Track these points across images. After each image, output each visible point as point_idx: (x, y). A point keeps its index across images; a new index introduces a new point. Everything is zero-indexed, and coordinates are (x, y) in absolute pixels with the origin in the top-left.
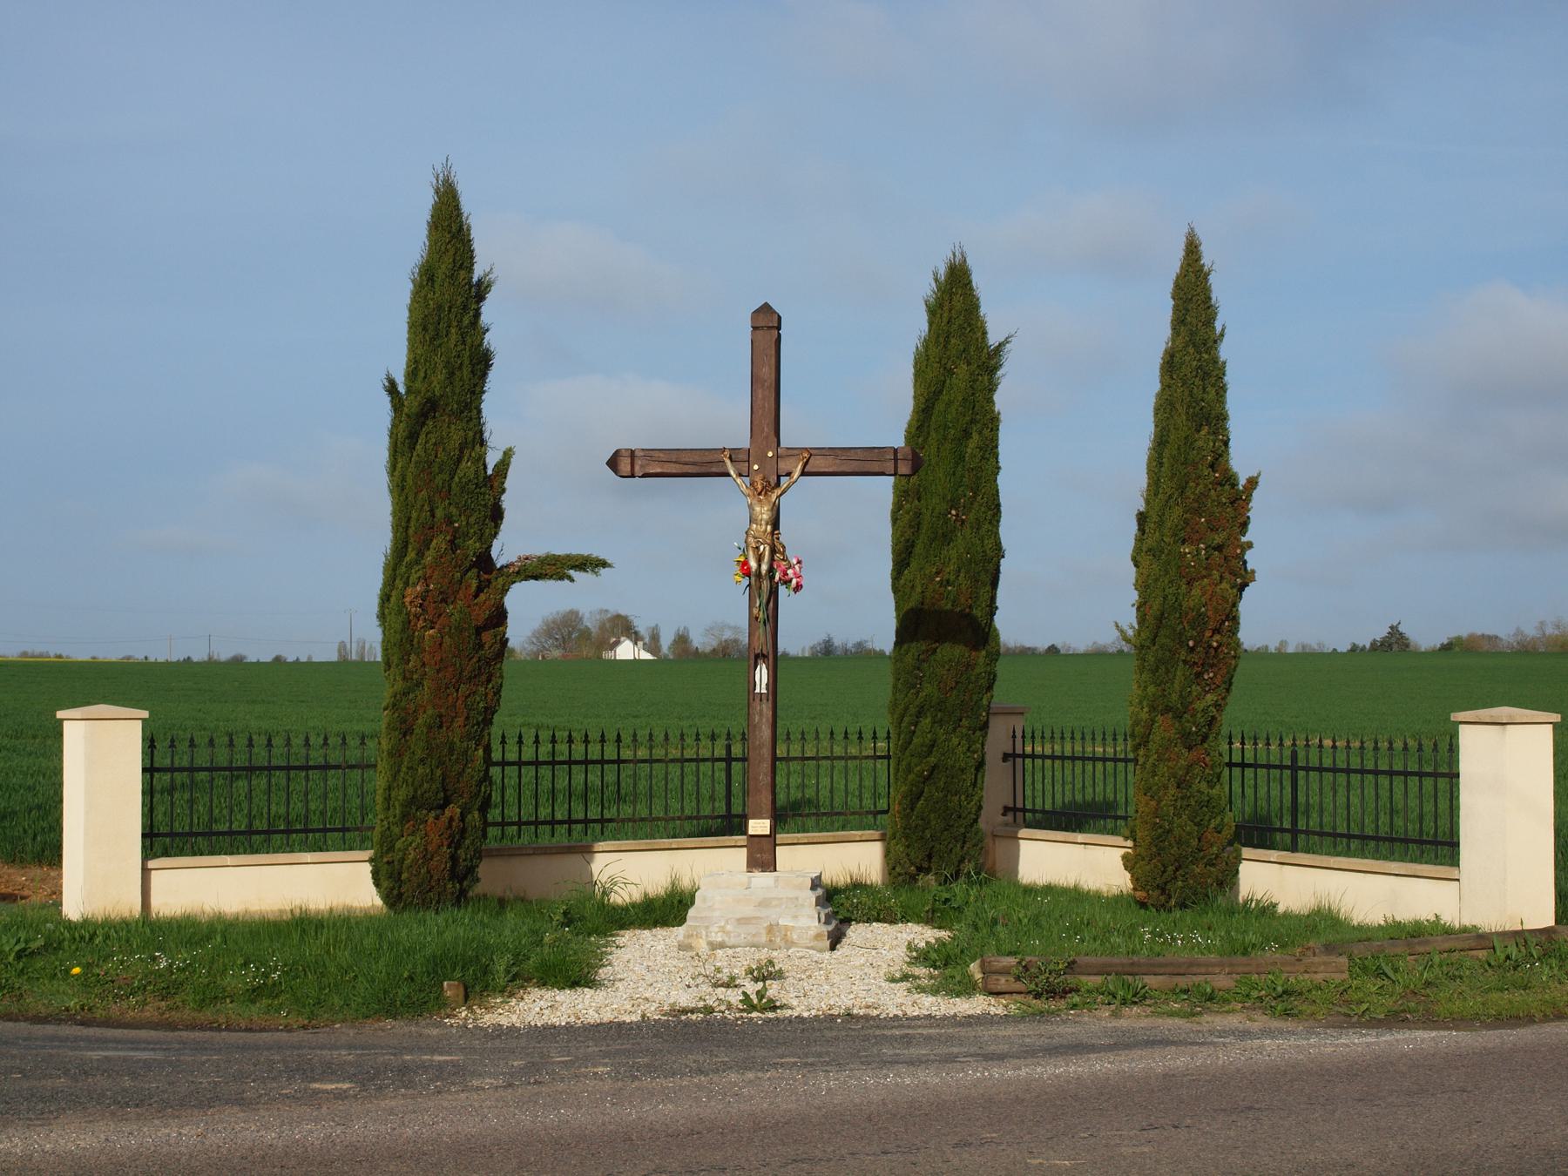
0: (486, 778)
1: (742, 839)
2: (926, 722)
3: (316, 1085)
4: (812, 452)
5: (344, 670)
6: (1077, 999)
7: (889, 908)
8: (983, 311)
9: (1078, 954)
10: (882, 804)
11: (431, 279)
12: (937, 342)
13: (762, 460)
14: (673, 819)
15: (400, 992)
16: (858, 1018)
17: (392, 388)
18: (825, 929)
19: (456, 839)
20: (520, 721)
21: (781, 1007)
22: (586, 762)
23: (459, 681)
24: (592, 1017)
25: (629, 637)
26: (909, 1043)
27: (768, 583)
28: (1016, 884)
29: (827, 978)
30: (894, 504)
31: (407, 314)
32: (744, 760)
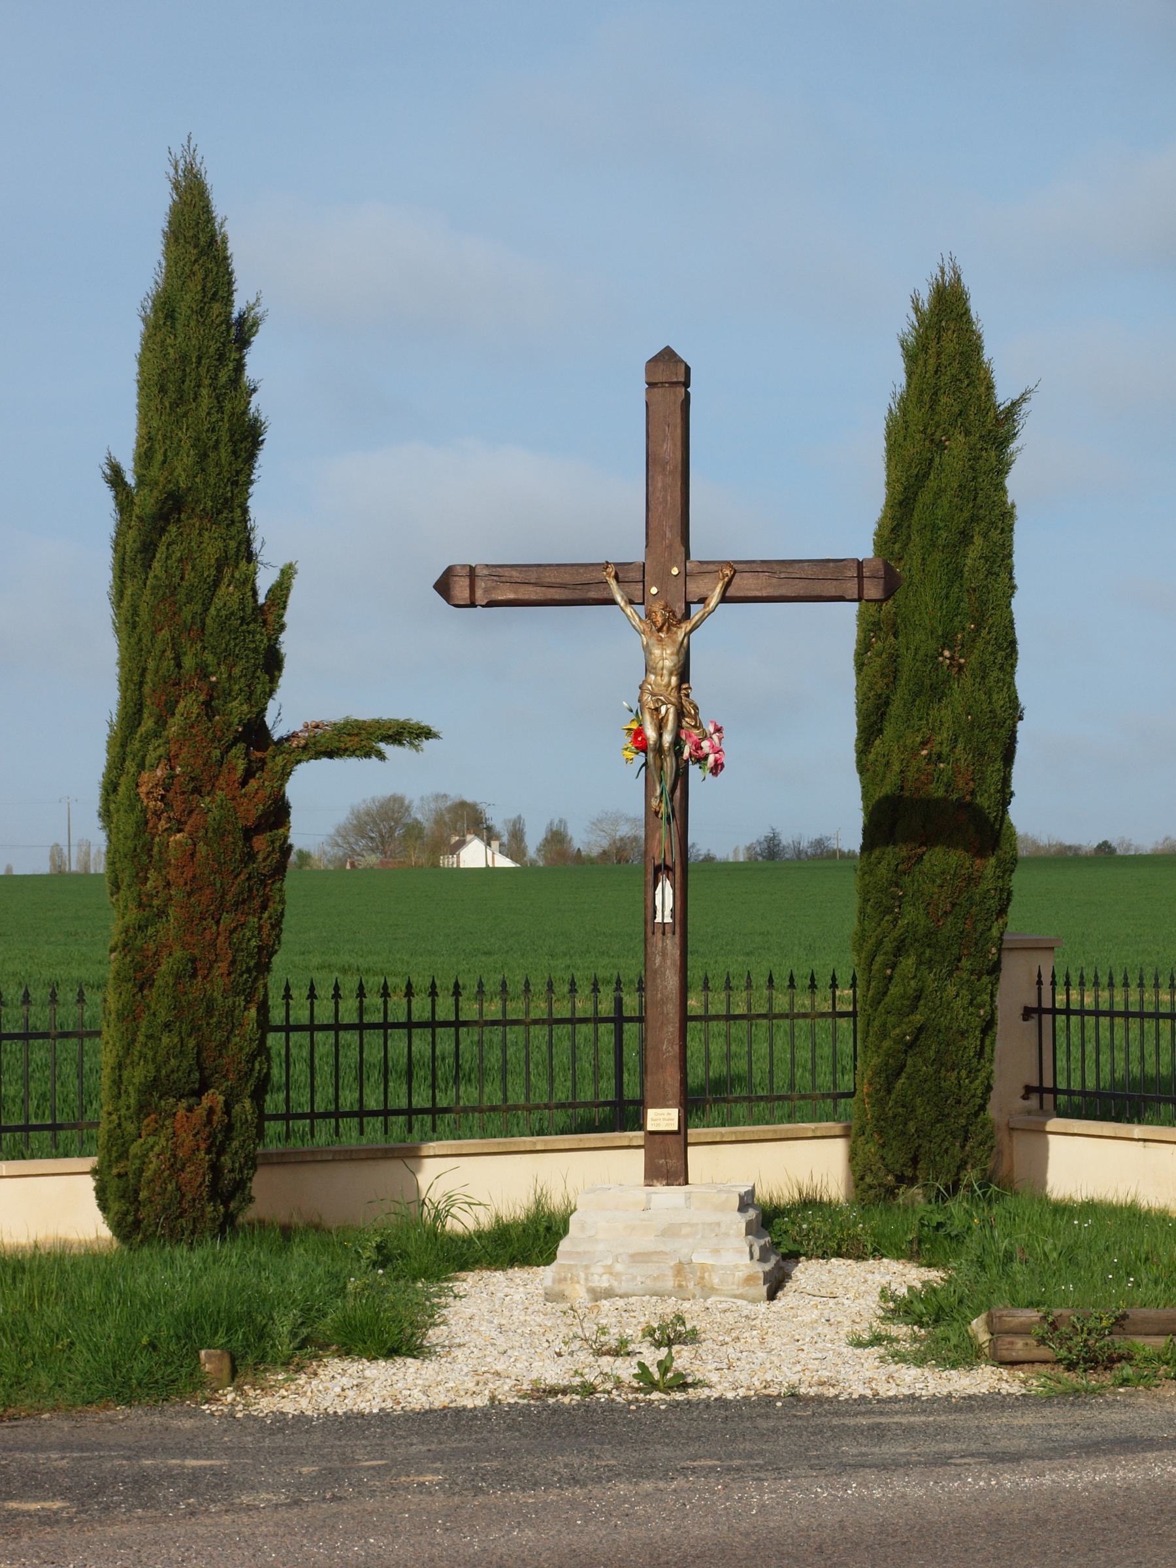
0: (262, 1049)
1: (637, 1137)
2: (908, 963)
3: (13, 1505)
4: (736, 568)
5: (58, 883)
6: (1128, 1371)
7: (855, 1237)
8: (987, 354)
9: (1131, 1305)
10: (846, 1082)
11: (170, 316)
12: (920, 401)
13: (663, 579)
14: (538, 1107)
15: (137, 1366)
16: (806, 1400)
17: (115, 478)
18: (760, 1269)
19: (219, 1138)
20: (316, 960)
21: (694, 1385)
22: (409, 1025)
23: (221, 908)
24: (418, 1401)
25: (478, 835)
26: (881, 1437)
27: (673, 759)
28: (1044, 1200)
29: (763, 1341)
30: (859, 642)
31: (135, 368)
32: (640, 1019)
